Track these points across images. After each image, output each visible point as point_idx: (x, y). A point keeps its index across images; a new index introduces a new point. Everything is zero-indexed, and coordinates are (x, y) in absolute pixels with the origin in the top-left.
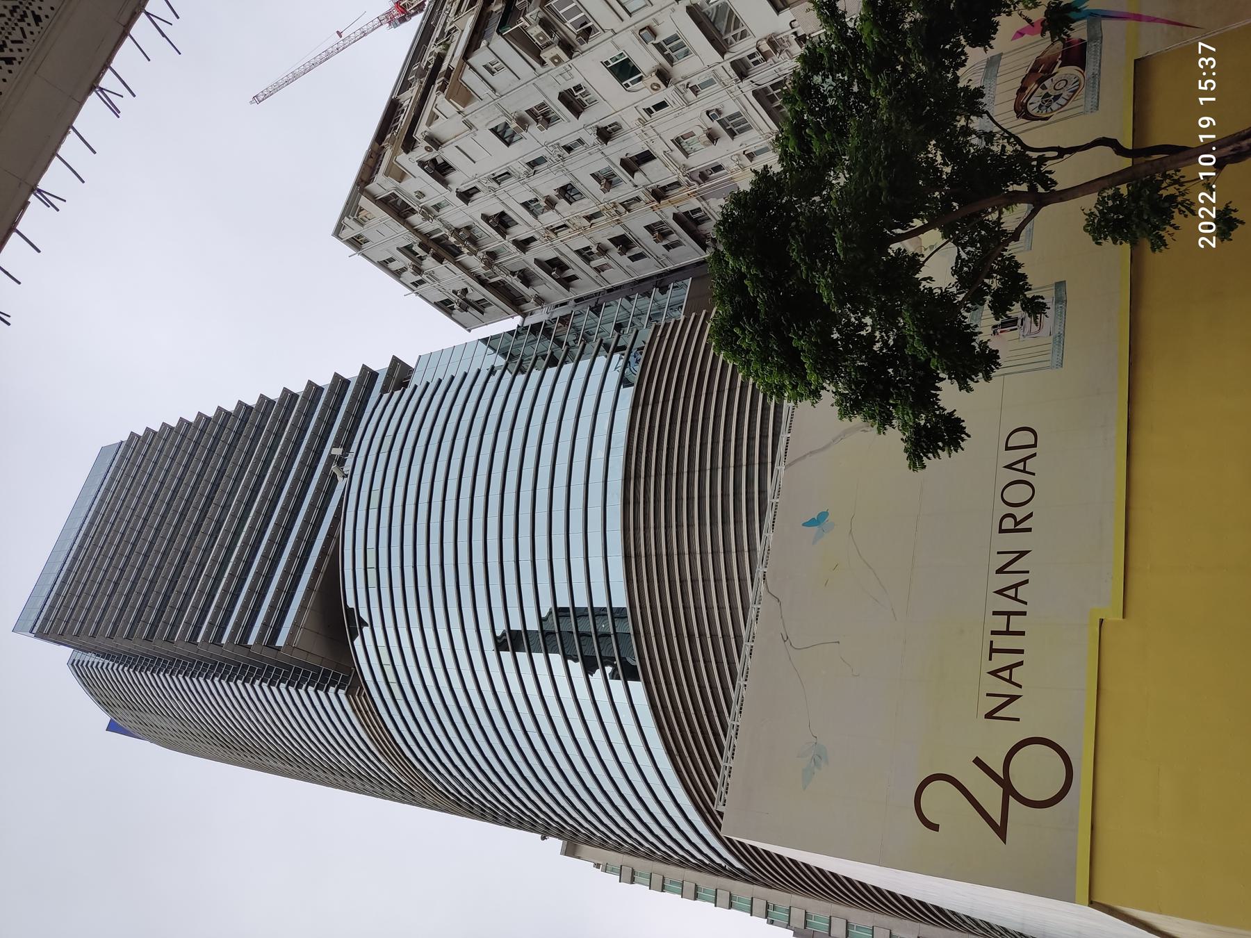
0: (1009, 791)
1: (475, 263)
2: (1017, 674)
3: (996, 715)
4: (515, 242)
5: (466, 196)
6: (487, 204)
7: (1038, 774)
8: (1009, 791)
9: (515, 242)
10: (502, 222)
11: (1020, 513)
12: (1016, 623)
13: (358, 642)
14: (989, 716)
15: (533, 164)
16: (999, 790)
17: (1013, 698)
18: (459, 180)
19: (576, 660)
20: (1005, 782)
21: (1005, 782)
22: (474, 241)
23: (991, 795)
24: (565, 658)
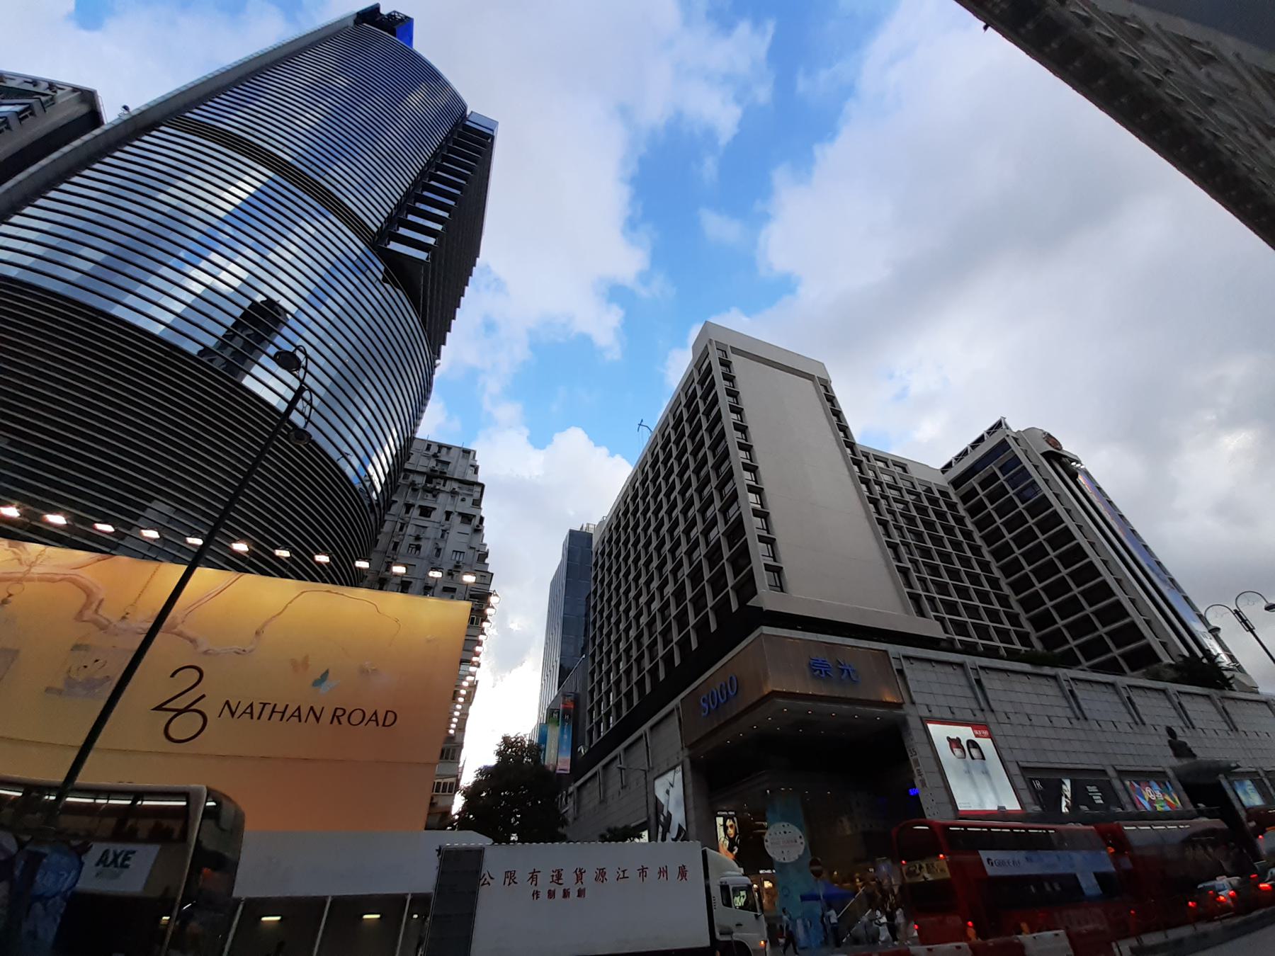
0: (180, 712)
1: (420, 480)
2: (296, 719)
3: (194, 707)
4: (413, 505)
5: (448, 514)
6: (438, 516)
7: (185, 726)
8: (180, 712)
9: (413, 505)
10: (426, 512)
11: (344, 719)
12: (277, 716)
13: (382, 268)
14: (227, 702)
15: (439, 550)
16: (182, 707)
17: (233, 714)
18: (456, 520)
19: (200, 352)
20: (187, 710)
21: (187, 710)
22: (426, 490)
23: (181, 703)
24: (206, 348)
